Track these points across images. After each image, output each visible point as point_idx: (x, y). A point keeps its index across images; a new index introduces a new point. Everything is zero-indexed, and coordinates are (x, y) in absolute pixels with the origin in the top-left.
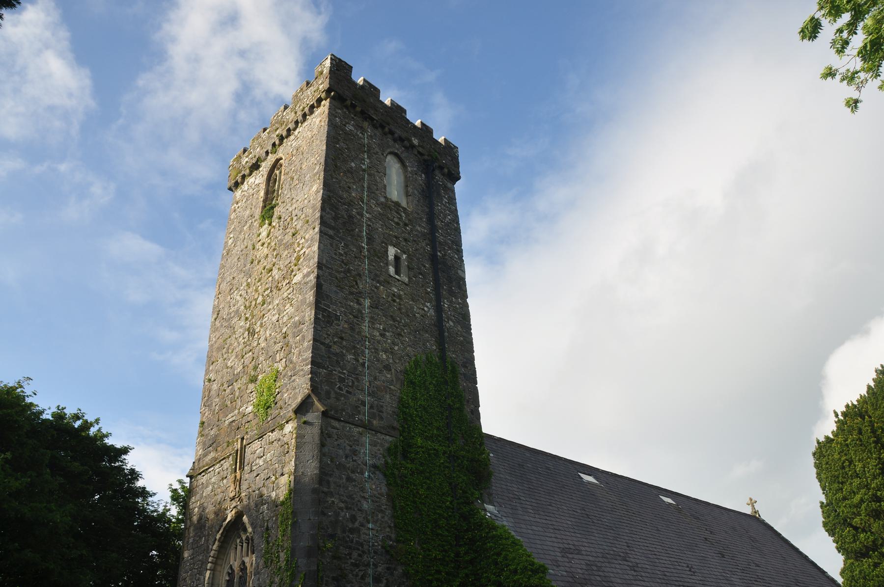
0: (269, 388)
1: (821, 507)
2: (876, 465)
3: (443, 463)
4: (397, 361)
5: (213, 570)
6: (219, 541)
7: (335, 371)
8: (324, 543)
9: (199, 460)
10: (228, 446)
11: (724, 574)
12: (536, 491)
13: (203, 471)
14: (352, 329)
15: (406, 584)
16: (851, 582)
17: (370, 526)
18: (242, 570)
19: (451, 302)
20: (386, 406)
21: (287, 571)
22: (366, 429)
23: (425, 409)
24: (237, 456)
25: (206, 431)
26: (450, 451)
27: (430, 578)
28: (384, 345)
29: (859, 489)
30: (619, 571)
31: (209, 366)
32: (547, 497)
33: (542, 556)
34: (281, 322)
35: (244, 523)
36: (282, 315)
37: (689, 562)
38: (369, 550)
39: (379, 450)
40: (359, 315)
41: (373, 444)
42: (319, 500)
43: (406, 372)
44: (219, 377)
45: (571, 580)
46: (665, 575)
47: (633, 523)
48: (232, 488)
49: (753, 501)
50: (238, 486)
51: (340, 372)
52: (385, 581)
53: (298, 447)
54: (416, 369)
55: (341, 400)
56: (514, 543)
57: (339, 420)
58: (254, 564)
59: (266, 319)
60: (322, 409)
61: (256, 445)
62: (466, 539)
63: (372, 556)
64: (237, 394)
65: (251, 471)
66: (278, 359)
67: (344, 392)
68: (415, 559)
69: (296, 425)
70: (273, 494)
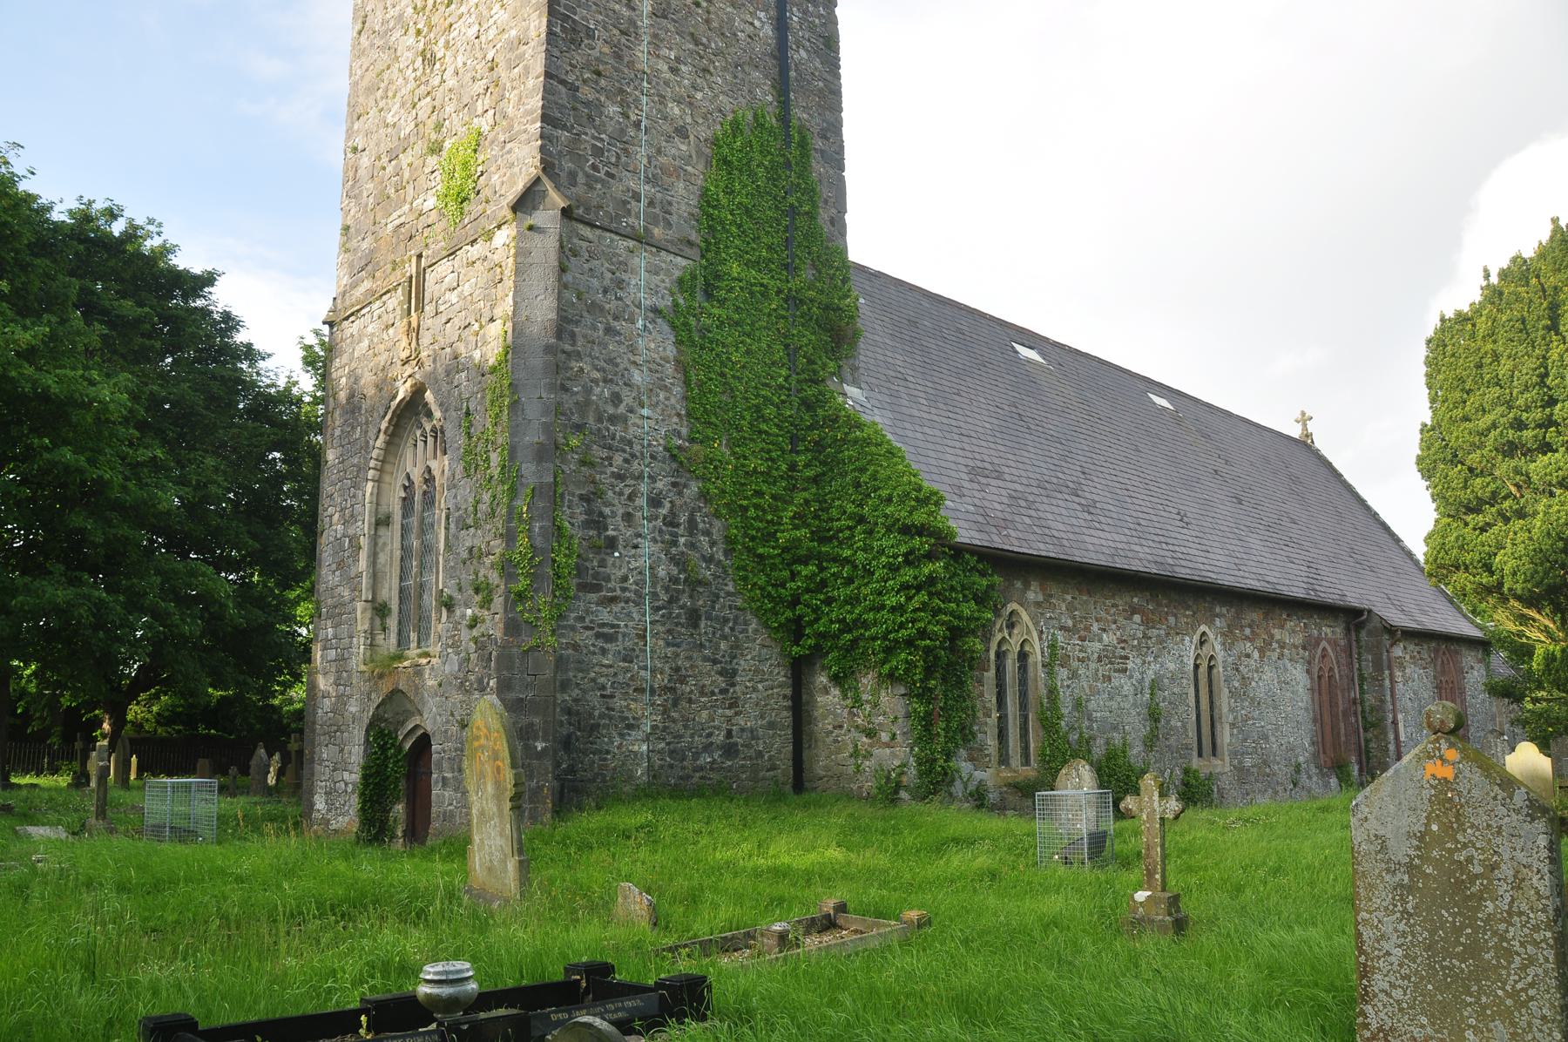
0: (465, 165)
1: (1422, 431)
2: (1535, 369)
3: (775, 310)
4: (701, 121)
5: (378, 481)
6: (385, 433)
7: (586, 134)
8: (565, 438)
9: (344, 294)
10: (394, 269)
11: (1236, 531)
12: (935, 368)
13: (352, 314)
14: (618, 56)
15: (704, 510)
16: (1439, 552)
17: (645, 412)
18: (426, 481)
19: (805, 12)
20: (678, 203)
21: (503, 483)
22: (642, 243)
23: (747, 211)
24: (410, 287)
25: (354, 244)
26: (790, 290)
27: (745, 503)
28: (678, 89)
29: (1494, 404)
30: (1064, 512)
31: (353, 123)
32: (954, 380)
33: (935, 477)
34: (483, 38)
35: (427, 404)
36: (485, 26)
37: (1181, 507)
38: (642, 453)
39: (663, 281)
40: (630, 30)
41: (654, 271)
42: (557, 366)
43: (715, 142)
44: (372, 144)
45: (980, 519)
46: (1139, 524)
47: (1098, 436)
48: (404, 343)
49: (1306, 417)
50: (414, 341)
51: (594, 138)
52: (668, 505)
53: (518, 272)
54: (734, 137)
55: (595, 189)
56: (891, 453)
57: (593, 226)
58: (446, 471)
59: (456, 33)
60: (563, 205)
61: (444, 267)
62: (809, 442)
63: (646, 463)
64: (406, 175)
65: (437, 314)
66: (480, 111)
67: (602, 175)
68: (720, 470)
69: (514, 233)
70: (477, 355)
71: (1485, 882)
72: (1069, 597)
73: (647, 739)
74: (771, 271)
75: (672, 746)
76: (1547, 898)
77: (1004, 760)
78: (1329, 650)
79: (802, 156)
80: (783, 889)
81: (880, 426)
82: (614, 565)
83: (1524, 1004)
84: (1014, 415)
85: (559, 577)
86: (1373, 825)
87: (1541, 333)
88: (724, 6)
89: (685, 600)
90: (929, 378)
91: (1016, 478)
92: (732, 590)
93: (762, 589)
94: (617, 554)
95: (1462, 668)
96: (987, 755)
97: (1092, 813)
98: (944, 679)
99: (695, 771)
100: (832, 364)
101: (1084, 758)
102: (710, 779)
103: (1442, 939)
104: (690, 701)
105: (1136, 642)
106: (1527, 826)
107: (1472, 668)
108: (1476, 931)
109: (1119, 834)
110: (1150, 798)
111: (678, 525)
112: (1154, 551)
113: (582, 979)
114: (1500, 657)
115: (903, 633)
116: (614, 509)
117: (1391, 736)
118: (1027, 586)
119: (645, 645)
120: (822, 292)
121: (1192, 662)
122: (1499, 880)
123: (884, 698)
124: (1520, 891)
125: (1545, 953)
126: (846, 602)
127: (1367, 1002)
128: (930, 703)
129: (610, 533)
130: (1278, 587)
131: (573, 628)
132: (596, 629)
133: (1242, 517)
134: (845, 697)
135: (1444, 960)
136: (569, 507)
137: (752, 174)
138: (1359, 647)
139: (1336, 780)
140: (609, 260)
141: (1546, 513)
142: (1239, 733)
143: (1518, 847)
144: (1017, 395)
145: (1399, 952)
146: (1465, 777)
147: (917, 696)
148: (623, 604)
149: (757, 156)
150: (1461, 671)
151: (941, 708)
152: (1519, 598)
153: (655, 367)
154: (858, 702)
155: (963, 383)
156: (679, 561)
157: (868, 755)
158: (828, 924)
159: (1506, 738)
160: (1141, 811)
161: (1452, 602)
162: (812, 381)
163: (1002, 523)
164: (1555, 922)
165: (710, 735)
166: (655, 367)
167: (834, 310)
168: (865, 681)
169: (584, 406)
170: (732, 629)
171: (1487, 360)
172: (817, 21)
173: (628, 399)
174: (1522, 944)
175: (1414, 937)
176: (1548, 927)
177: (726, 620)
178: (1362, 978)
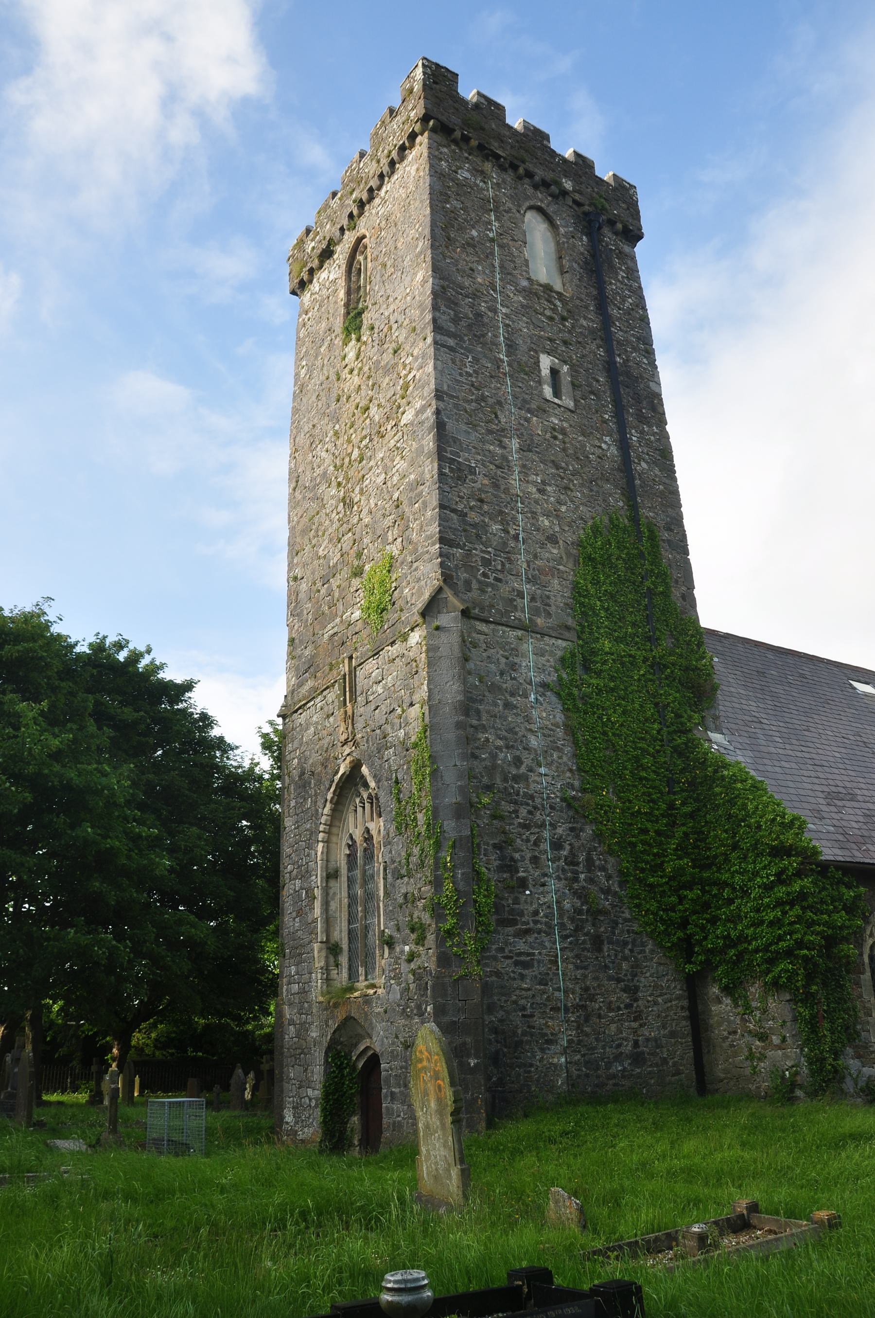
3: (643, 675)
4: (567, 528)
7: (476, 549)
12: (785, 710)
14: (496, 486)
17: (543, 770)
19: (642, 432)
20: (555, 596)
22: (528, 631)
33: (797, 804)
38: (543, 805)
39: (548, 661)
40: (504, 464)
41: (539, 653)
43: (579, 544)
45: (841, 838)
52: (568, 847)
54: (595, 537)
56: (755, 787)
57: (487, 622)
60: (462, 607)
62: (684, 783)
67: (491, 580)
68: (610, 814)
73: (564, 1052)
74: (637, 643)
79: (653, 546)
82: (526, 902)
85: (480, 915)
89: (589, 928)
91: (867, 799)
93: (655, 914)
94: (528, 892)
98: (825, 984)
100: (696, 715)
102: (623, 1086)
104: (600, 1017)
111: (578, 864)
116: (523, 853)
119: (558, 969)
120: (681, 656)
123: (772, 1004)
126: (729, 920)
129: (521, 874)
132: (515, 958)
134: (736, 1006)
136: (485, 855)
140: (503, 648)
144: (860, 726)
147: (802, 1001)
151: (825, 1011)
153: (547, 732)
154: (747, 1007)
156: (581, 895)
157: (763, 1057)
163: (861, 840)
165: (619, 1046)
166: (547, 732)
167: (693, 670)
168: (753, 990)
169: (492, 769)
170: (631, 951)
172: (652, 438)
173: (527, 760)
177: (625, 944)
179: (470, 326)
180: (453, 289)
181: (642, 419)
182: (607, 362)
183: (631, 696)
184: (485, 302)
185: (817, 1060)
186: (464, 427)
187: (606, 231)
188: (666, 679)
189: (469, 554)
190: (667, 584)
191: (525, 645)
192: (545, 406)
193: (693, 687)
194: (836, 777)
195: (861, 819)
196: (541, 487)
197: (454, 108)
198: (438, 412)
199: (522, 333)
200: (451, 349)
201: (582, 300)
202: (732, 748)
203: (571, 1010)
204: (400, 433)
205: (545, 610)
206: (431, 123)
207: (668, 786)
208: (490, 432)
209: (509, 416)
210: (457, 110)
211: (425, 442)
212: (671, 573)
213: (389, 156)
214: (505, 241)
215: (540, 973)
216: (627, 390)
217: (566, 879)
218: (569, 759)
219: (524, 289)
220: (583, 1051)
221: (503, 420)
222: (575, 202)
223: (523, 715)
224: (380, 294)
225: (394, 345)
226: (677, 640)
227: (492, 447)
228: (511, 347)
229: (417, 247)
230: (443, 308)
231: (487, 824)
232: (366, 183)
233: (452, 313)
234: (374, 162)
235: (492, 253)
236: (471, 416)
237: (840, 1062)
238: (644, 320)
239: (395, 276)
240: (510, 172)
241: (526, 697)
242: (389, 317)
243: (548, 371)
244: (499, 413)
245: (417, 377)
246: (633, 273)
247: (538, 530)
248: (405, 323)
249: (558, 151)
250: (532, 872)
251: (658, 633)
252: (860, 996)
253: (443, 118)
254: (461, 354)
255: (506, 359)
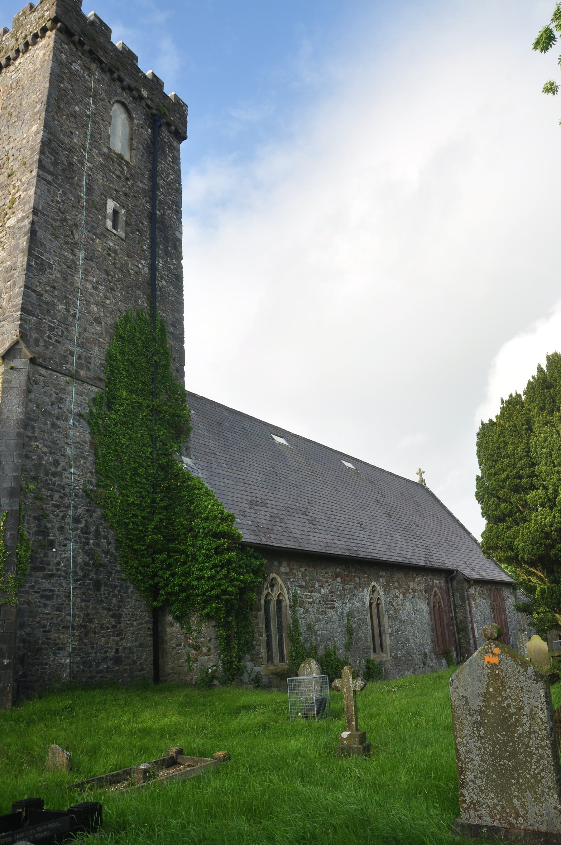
1: (477, 479)
2: (524, 449)
3: (145, 416)
4: (108, 315)
7: (45, 319)
11: (389, 531)
12: (231, 448)
14: (65, 279)
16: (488, 540)
17: (72, 470)
19: (166, 262)
20: (94, 358)
22: (73, 378)
27: (127, 521)
28: (96, 298)
29: (507, 466)
30: (299, 523)
33: (231, 506)
37: (360, 520)
38: (70, 493)
39: (85, 399)
40: (72, 266)
41: (79, 393)
43: (116, 326)
45: (255, 529)
46: (339, 530)
51: (50, 321)
52: (84, 522)
54: (126, 324)
56: (207, 493)
57: (46, 368)
60: (30, 356)
62: (163, 487)
67: (53, 341)
68: (114, 503)
71: (517, 717)
72: (303, 570)
73: (69, 656)
74: (143, 395)
75: (84, 659)
76: (546, 723)
77: (270, 658)
78: (438, 592)
79: (162, 335)
80: (147, 742)
81: (201, 479)
82: (52, 556)
83: (540, 781)
84: (273, 473)
85: (20, 563)
86: (461, 690)
87: (524, 432)
88: (123, 256)
89: (93, 575)
90: (227, 453)
91: (273, 506)
92: (120, 569)
93: (136, 568)
94: (54, 550)
95: (504, 598)
96: (261, 658)
97: (318, 688)
98: (237, 617)
99: (98, 673)
100: (176, 446)
101: (313, 657)
102: (106, 677)
103: (498, 749)
104: (95, 633)
105: (339, 592)
106: (535, 686)
107: (508, 597)
108: (514, 744)
109: (333, 698)
110: (348, 680)
111: (89, 533)
112: (347, 544)
113: (23, 811)
114: (521, 591)
115: (214, 592)
116: (53, 524)
117: (471, 636)
118: (280, 564)
119: (70, 601)
120: (170, 407)
121: (368, 601)
122: (524, 715)
123: (204, 628)
124: (534, 720)
125: (547, 752)
126: (182, 575)
127: (464, 788)
128: (229, 630)
129: (51, 538)
130: (411, 560)
131: (27, 592)
132: (41, 593)
133: (391, 524)
134: (182, 628)
135: (500, 761)
136: (27, 523)
137: (135, 344)
138: (453, 590)
139: (445, 661)
140: (55, 387)
141: (535, 520)
142: (394, 638)
143: (531, 697)
144: (274, 462)
145: (478, 758)
146: (504, 662)
147: (222, 626)
148: (57, 578)
149: (138, 335)
150: (503, 600)
151: (235, 632)
152: (525, 563)
153: (78, 446)
154: (189, 629)
155: (245, 455)
156: (90, 554)
157: (196, 660)
158: (172, 762)
159: (526, 633)
160: (343, 687)
161: (497, 564)
162: (165, 454)
163: (267, 531)
164: (551, 735)
165: (106, 652)
166: (78, 446)
167: (177, 417)
168: (193, 619)
169: (38, 467)
170: (119, 591)
171: (502, 445)
172: (172, 266)
173: (63, 464)
174: (537, 749)
175: (485, 750)
176: (548, 738)
177: (116, 586)
178: (461, 774)
179: (64, 170)
180: (56, 142)
181: (167, 253)
182: (151, 213)
183: (136, 429)
184: (77, 156)
185: (228, 663)
186: (49, 237)
187: (164, 129)
188: (160, 420)
189: (40, 322)
190: (168, 360)
191: (71, 387)
192: (106, 233)
193: (176, 427)
194: (256, 491)
195: (268, 518)
196: (95, 285)
197: (77, 19)
198: (33, 223)
199: (98, 183)
200: (49, 182)
201: (141, 170)
202: (195, 468)
203: (76, 628)
204: (4, 232)
205: (87, 366)
206: (59, 25)
207: (153, 488)
208: (66, 243)
209: (81, 235)
210: (79, 21)
211: (20, 242)
212: (171, 353)
213: (25, 39)
214: (97, 119)
215: (57, 604)
216: (161, 233)
217: (80, 543)
218: (91, 465)
219: (104, 154)
220: (82, 655)
221: (77, 237)
222: (147, 105)
223: (63, 433)
224: (4, 134)
225: (9, 171)
226: (170, 396)
227: (66, 253)
228: (90, 190)
229: (36, 108)
230: (47, 153)
231: (31, 503)
232: (5, 52)
233: (53, 158)
234: (13, 39)
235: (87, 125)
236: (55, 230)
237: (241, 664)
238: (179, 191)
239: (17, 124)
240: (108, 74)
241: (67, 420)
242: (8, 151)
243: (112, 211)
244: (74, 231)
245: (22, 196)
246: (176, 160)
247: (89, 313)
248: (19, 158)
249: (142, 70)
250: (58, 536)
251: (158, 390)
252: (257, 624)
253: (68, 24)
254: (55, 187)
255: (84, 197)
